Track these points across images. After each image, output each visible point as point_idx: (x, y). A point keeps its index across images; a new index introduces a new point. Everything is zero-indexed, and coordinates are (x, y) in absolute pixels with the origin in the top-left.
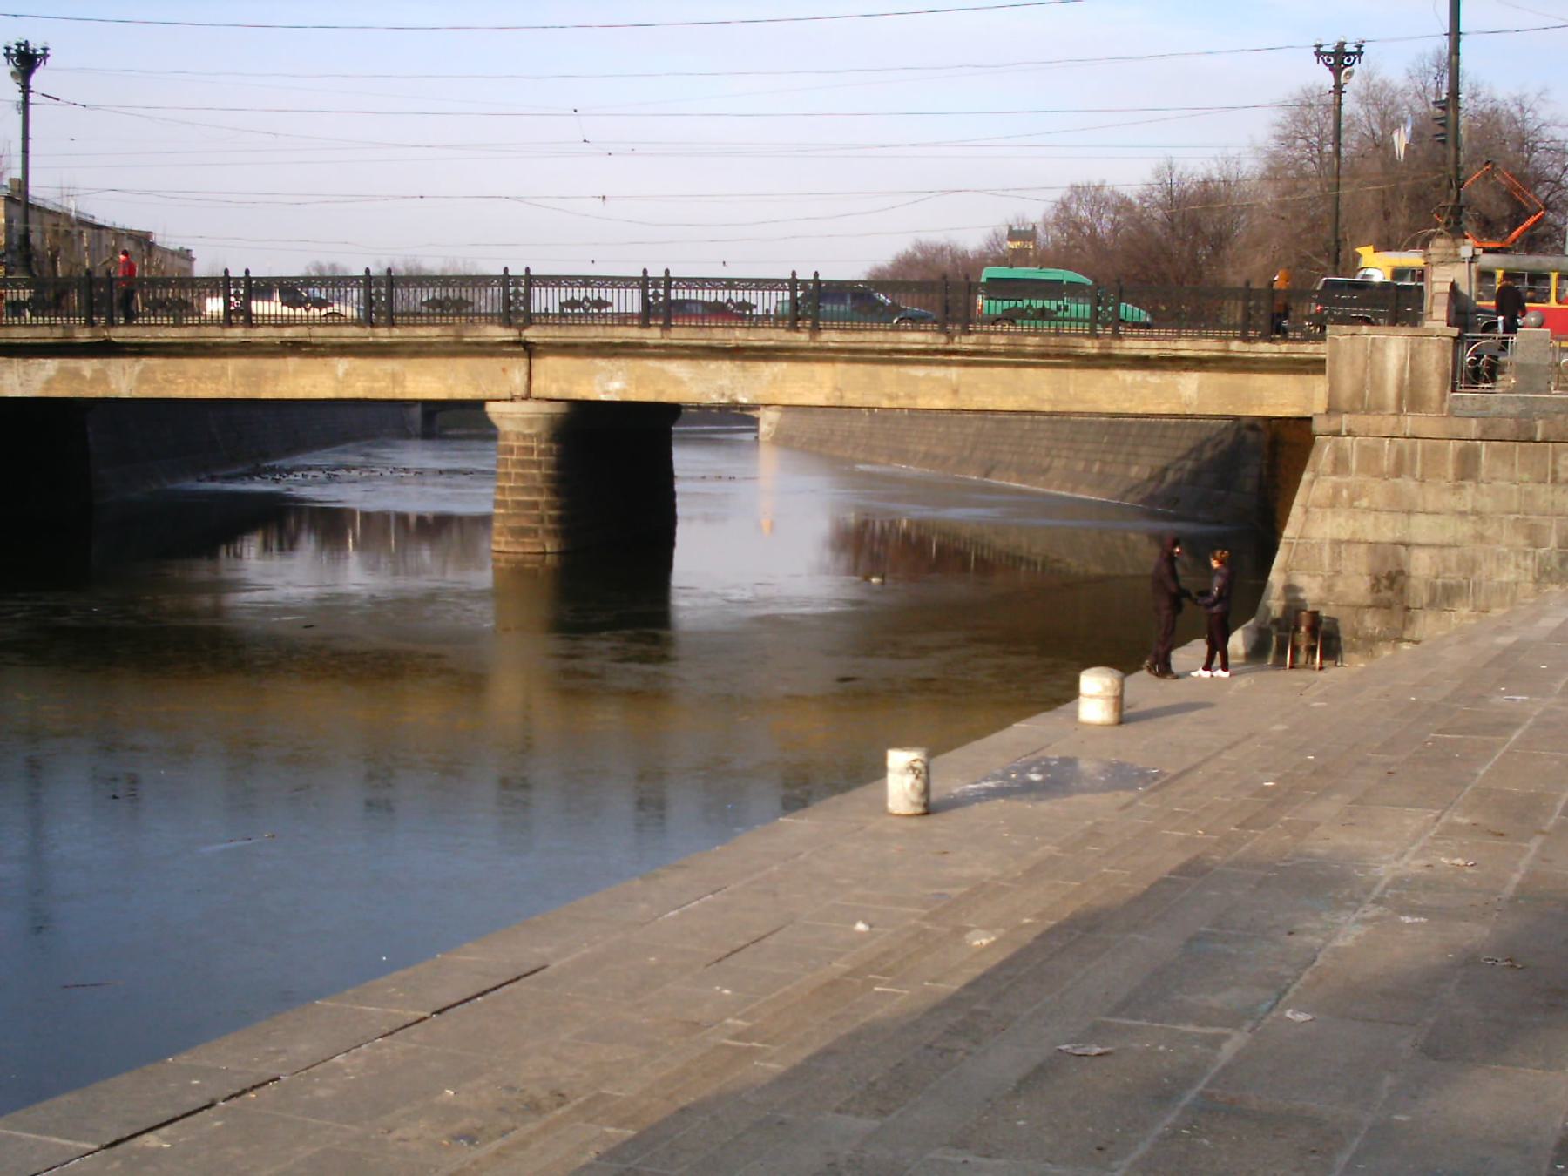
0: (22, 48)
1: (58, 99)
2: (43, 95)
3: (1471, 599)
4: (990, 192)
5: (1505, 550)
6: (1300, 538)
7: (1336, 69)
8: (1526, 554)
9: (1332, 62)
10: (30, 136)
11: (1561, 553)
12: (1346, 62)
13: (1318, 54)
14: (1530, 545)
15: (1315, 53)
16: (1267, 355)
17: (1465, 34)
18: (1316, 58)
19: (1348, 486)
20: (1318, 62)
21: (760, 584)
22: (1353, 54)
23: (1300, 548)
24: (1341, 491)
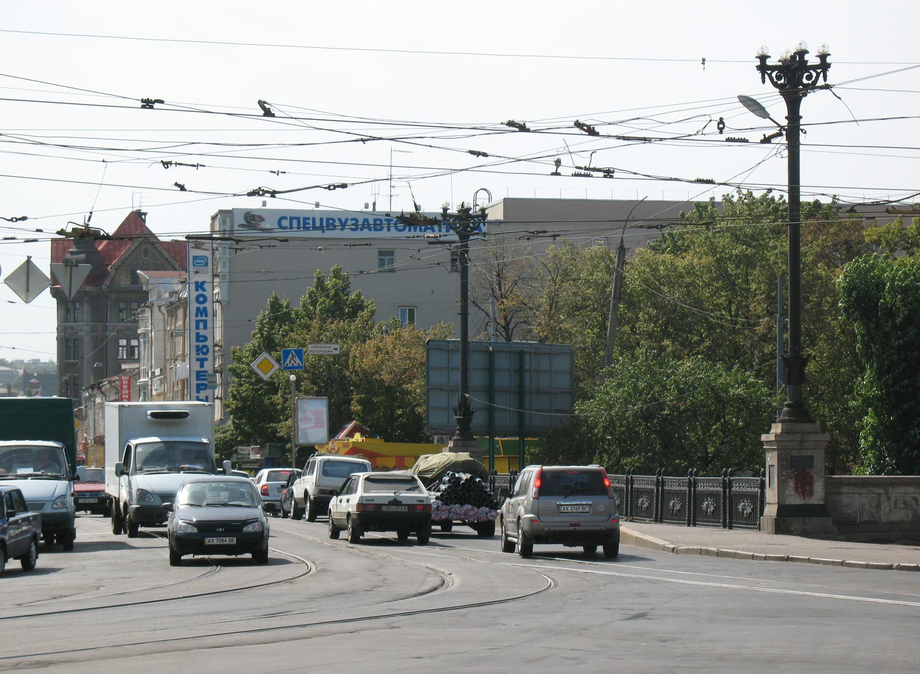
4: (767, 158)
10: (459, 318)
12: (805, 81)
13: (763, 68)
15: (759, 68)
20: (764, 82)
21: (368, 591)
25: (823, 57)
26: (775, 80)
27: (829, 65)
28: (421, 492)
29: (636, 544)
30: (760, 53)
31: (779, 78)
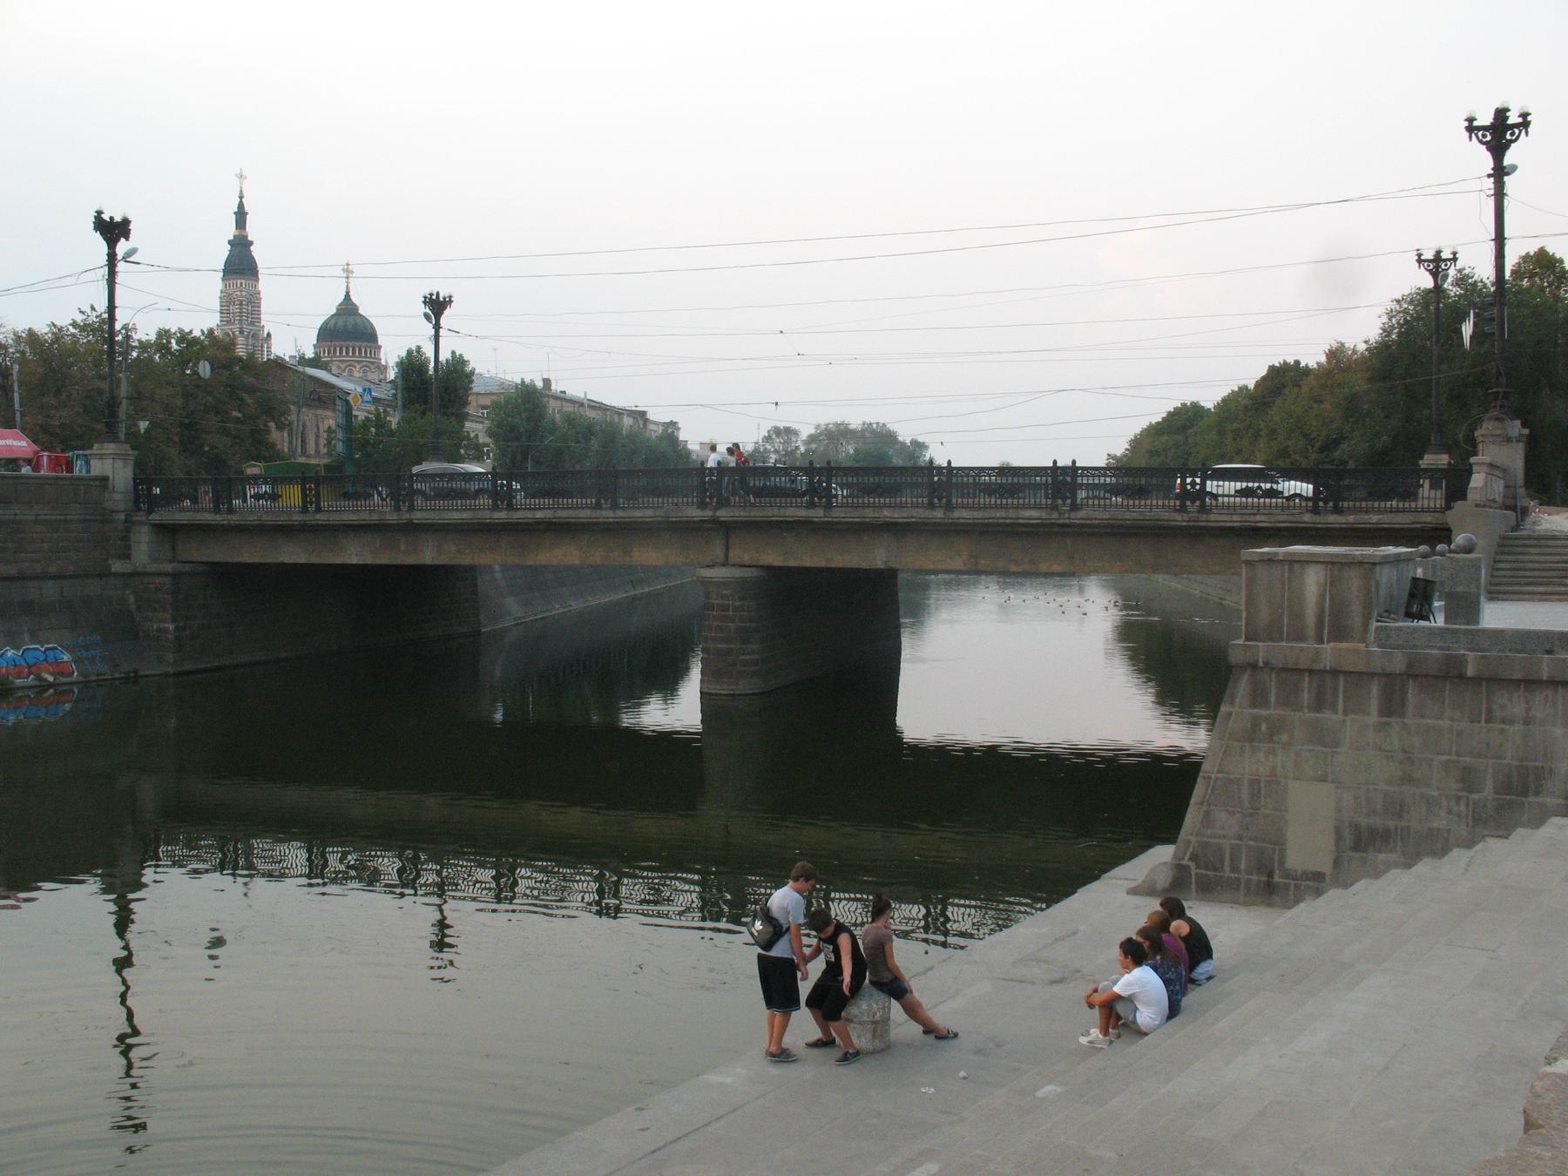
0: (434, 297)
1: (458, 333)
2: (449, 330)
3: (1399, 844)
5: (1436, 793)
6: (1218, 772)
8: (1458, 799)
9: (1431, 267)
11: (1497, 799)
12: (1443, 267)
14: (1463, 790)
16: (1337, 526)
17: (1509, 239)
18: (1417, 265)
19: (1266, 719)
20: (1470, 140)
22: (1449, 260)
23: (1219, 783)
24: (1260, 725)
25: (1524, 115)
26: (1481, 138)
27: (1457, 259)
28: (1431, 622)
29: (405, 389)
30: (1469, 116)
31: (1429, 266)
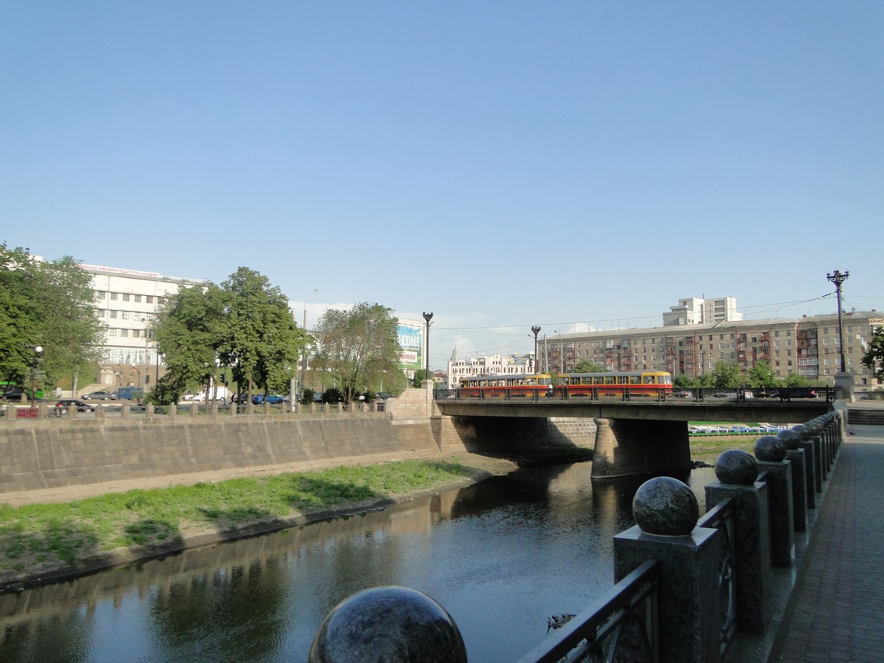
2: (305, 311)
7: (838, 284)
15: (827, 277)
